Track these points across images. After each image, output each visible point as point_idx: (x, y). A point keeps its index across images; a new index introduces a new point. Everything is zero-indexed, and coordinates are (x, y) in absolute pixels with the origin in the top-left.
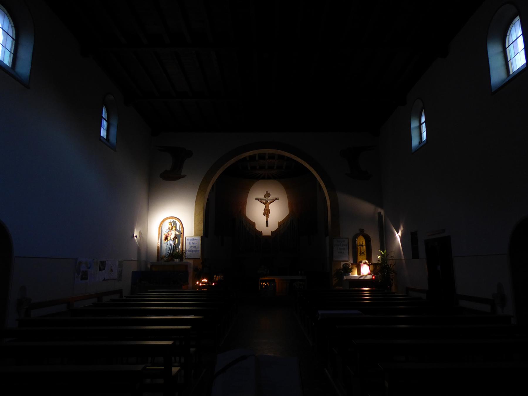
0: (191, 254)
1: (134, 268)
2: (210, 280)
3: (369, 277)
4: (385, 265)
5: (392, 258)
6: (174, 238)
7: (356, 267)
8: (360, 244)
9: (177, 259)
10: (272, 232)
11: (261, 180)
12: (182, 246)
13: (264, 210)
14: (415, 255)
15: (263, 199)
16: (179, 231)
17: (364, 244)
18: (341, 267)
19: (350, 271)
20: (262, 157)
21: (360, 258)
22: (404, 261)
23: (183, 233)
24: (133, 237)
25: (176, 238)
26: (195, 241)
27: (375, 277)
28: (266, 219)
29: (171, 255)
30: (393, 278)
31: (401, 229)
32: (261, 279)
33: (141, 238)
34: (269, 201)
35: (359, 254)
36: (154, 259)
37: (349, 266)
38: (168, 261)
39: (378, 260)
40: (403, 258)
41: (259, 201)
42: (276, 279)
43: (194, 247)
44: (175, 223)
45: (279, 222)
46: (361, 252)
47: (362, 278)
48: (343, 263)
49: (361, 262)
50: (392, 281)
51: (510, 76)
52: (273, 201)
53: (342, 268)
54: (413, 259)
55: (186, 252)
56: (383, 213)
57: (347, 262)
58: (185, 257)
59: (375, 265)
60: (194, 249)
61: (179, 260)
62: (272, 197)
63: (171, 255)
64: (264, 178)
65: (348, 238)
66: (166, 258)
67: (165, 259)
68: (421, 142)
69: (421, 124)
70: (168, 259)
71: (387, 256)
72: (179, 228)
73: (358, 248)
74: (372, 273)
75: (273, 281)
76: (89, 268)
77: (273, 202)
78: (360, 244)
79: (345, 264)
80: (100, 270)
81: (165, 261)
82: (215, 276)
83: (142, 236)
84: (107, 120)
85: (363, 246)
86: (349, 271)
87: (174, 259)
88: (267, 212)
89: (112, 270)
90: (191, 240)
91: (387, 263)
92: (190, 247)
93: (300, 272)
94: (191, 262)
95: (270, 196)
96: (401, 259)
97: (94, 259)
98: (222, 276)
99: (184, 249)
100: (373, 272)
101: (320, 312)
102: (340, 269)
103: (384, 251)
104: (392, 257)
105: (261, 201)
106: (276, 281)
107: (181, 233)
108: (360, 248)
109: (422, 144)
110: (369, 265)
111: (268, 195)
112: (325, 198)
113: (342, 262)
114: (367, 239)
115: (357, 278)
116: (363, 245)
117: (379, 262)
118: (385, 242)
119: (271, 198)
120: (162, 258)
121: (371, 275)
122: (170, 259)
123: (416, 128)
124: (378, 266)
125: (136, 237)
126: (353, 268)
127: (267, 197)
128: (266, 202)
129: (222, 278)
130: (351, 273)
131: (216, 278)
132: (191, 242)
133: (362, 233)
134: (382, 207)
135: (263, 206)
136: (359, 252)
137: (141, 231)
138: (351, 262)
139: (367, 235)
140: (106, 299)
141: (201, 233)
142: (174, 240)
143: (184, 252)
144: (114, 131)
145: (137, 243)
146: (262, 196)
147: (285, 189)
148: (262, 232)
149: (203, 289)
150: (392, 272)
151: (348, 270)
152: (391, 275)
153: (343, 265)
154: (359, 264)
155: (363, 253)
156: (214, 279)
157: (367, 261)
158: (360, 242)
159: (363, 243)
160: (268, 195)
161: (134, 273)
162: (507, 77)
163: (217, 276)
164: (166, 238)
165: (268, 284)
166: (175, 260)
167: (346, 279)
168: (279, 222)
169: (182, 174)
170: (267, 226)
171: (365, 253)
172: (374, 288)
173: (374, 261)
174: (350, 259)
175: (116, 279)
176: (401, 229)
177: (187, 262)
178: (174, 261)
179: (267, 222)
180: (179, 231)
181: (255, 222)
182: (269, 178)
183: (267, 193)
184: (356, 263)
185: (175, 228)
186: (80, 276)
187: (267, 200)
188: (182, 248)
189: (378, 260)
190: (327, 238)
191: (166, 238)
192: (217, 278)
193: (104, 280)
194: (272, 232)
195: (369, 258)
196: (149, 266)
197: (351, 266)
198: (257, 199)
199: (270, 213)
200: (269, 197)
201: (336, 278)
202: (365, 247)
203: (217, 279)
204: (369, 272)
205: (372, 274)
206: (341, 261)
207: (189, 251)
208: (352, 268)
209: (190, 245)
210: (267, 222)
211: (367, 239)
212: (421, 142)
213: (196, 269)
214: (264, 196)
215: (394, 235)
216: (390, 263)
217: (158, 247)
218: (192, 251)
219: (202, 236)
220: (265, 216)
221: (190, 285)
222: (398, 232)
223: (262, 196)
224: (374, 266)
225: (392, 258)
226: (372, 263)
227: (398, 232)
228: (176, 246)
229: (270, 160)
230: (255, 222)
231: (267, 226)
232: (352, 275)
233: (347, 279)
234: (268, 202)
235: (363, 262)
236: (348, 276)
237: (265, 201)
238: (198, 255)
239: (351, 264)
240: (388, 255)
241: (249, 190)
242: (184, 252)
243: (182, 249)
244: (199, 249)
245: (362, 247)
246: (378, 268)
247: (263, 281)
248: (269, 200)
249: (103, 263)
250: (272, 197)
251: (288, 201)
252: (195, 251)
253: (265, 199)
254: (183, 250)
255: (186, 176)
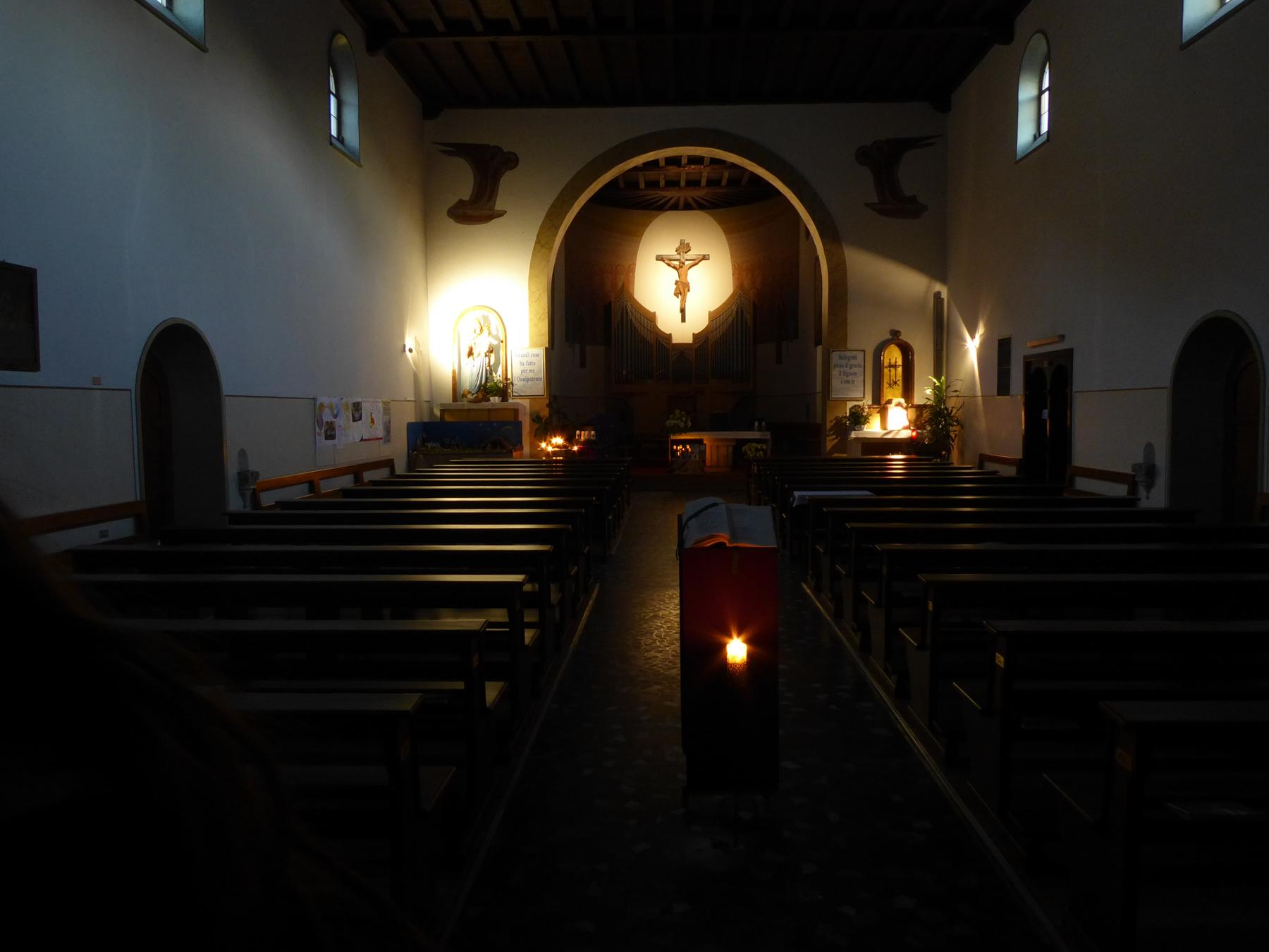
0: (524, 385)
1: (409, 415)
2: (570, 439)
3: (906, 434)
4: (940, 408)
5: (955, 394)
6: (488, 351)
7: (878, 412)
8: (890, 363)
9: (497, 398)
10: (694, 334)
11: (669, 212)
12: (504, 368)
13: (676, 284)
14: (1003, 387)
15: (672, 257)
16: (496, 337)
17: (900, 362)
18: (846, 413)
19: (865, 420)
20: (674, 161)
21: (888, 393)
22: (980, 400)
23: (504, 342)
24: (405, 351)
25: (491, 352)
26: (534, 359)
27: (917, 433)
28: (681, 305)
29: (482, 388)
30: (956, 435)
31: (981, 331)
32: (673, 437)
33: (418, 353)
34: (687, 263)
35: (886, 385)
36: (447, 398)
37: (863, 409)
38: (476, 401)
39: (927, 398)
40: (979, 393)
41: (664, 261)
42: (707, 438)
43: (530, 371)
44: (486, 319)
45: (709, 312)
46: (892, 382)
47: (889, 436)
48: (850, 405)
49: (889, 402)
50: (953, 441)
51: (1225, 6)
52: (696, 261)
53: (848, 415)
54: (998, 395)
55: (514, 382)
56: (944, 295)
57: (860, 403)
58: (512, 392)
59: (920, 408)
60: (530, 375)
61: (501, 398)
62: (695, 252)
63: (482, 388)
64: (675, 207)
65: (864, 351)
66: (473, 395)
67: (469, 396)
68: (1037, 136)
69: (1041, 93)
70: (476, 397)
71: (948, 387)
72: (497, 330)
73: (886, 371)
74: (912, 425)
75: (700, 442)
76: (335, 417)
77: (696, 264)
78: (890, 363)
79: (855, 406)
80: (354, 420)
81: (470, 401)
82: (578, 432)
83: (420, 349)
84: (334, 92)
85: (895, 366)
86: (862, 420)
87: (488, 396)
88: (682, 289)
89: (373, 421)
90: (523, 356)
91: (945, 404)
92: (523, 371)
93: (756, 424)
94: (526, 403)
95: (690, 250)
96: (975, 396)
97: (342, 399)
98: (593, 432)
99: (509, 376)
100: (917, 424)
101: (797, 494)
102: (841, 418)
103: (941, 378)
104: (956, 391)
105: (669, 262)
106: (705, 442)
107: (502, 342)
108: (890, 371)
109: (1040, 141)
110: (906, 408)
111: (684, 247)
112: (817, 259)
113: (848, 403)
114: (907, 351)
115: (879, 436)
116: (896, 365)
117: (928, 403)
118: (945, 359)
119: (691, 254)
120: (464, 396)
121: (910, 428)
122: (480, 396)
123: (1032, 99)
124: (925, 411)
125: (411, 351)
126: (871, 415)
127: (683, 252)
128: (682, 265)
129: (593, 436)
130: (866, 426)
131: (580, 435)
132: (525, 360)
133: (895, 338)
134: (944, 281)
135: (674, 275)
136: (886, 380)
137: (417, 338)
138: (868, 401)
139: (906, 343)
140: (327, 487)
141: (545, 340)
142: (486, 356)
143: (509, 382)
144: (351, 118)
145: (411, 362)
146: (670, 250)
147: (725, 234)
148: (670, 334)
149: (554, 458)
150: (955, 423)
151: (858, 418)
152: (951, 428)
153: (851, 409)
154: (884, 407)
155: (895, 383)
156: (577, 437)
157: (902, 401)
158: (890, 360)
159: (896, 362)
160: (684, 247)
161: (411, 427)
162: (1218, 6)
163: (583, 432)
164: (470, 353)
165: (688, 450)
166: (491, 398)
167: (855, 438)
168: (709, 312)
169: (499, 206)
170: (683, 320)
171: (900, 383)
172: (913, 456)
173: (918, 400)
174: (866, 396)
175: (381, 438)
176: (981, 331)
177: (518, 403)
178: (490, 400)
179: (683, 311)
180: (496, 337)
181: (655, 313)
182: (688, 207)
183: (682, 243)
184: (879, 404)
185: (489, 330)
186: (323, 431)
187: (683, 260)
188: (504, 373)
189: (927, 398)
190: (819, 348)
191: (470, 353)
192: (583, 435)
193: (362, 440)
194: (694, 334)
195: (908, 392)
196: (437, 412)
197: (866, 410)
198: (660, 258)
199: (689, 290)
200: (686, 253)
201: (834, 437)
202: (900, 370)
203: (582, 438)
204: (907, 423)
205: (912, 428)
206: (845, 400)
207: (521, 380)
208: (869, 415)
209: (523, 368)
210: (683, 311)
211: (907, 351)
212: (1037, 136)
213: (536, 418)
214: (676, 251)
215: (963, 339)
216: (951, 403)
217: (454, 372)
218: (527, 380)
219: (546, 348)
220: (678, 297)
221: (527, 450)
222: (973, 337)
223: (670, 250)
224: (917, 411)
225: (955, 394)
226: (912, 405)
227: (973, 337)
228: (490, 371)
229: (693, 167)
230: (655, 313)
231: (683, 320)
232: (867, 430)
233: (857, 439)
234: (684, 264)
235: (895, 401)
236: (860, 432)
237: (677, 263)
238: (539, 388)
239: (867, 407)
240: (949, 386)
241: (641, 236)
242: (509, 382)
243: (504, 377)
244: (542, 375)
245: (893, 370)
246: (926, 414)
247: (678, 442)
248: (687, 260)
249: (357, 407)
250: (695, 252)
251: (732, 262)
252: (532, 379)
253: (678, 257)
254: (507, 379)
255: (506, 212)
